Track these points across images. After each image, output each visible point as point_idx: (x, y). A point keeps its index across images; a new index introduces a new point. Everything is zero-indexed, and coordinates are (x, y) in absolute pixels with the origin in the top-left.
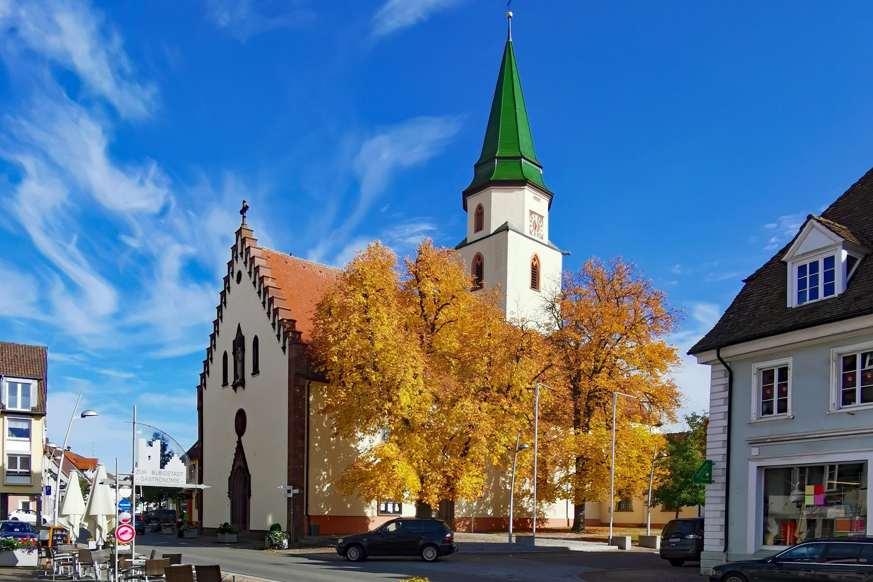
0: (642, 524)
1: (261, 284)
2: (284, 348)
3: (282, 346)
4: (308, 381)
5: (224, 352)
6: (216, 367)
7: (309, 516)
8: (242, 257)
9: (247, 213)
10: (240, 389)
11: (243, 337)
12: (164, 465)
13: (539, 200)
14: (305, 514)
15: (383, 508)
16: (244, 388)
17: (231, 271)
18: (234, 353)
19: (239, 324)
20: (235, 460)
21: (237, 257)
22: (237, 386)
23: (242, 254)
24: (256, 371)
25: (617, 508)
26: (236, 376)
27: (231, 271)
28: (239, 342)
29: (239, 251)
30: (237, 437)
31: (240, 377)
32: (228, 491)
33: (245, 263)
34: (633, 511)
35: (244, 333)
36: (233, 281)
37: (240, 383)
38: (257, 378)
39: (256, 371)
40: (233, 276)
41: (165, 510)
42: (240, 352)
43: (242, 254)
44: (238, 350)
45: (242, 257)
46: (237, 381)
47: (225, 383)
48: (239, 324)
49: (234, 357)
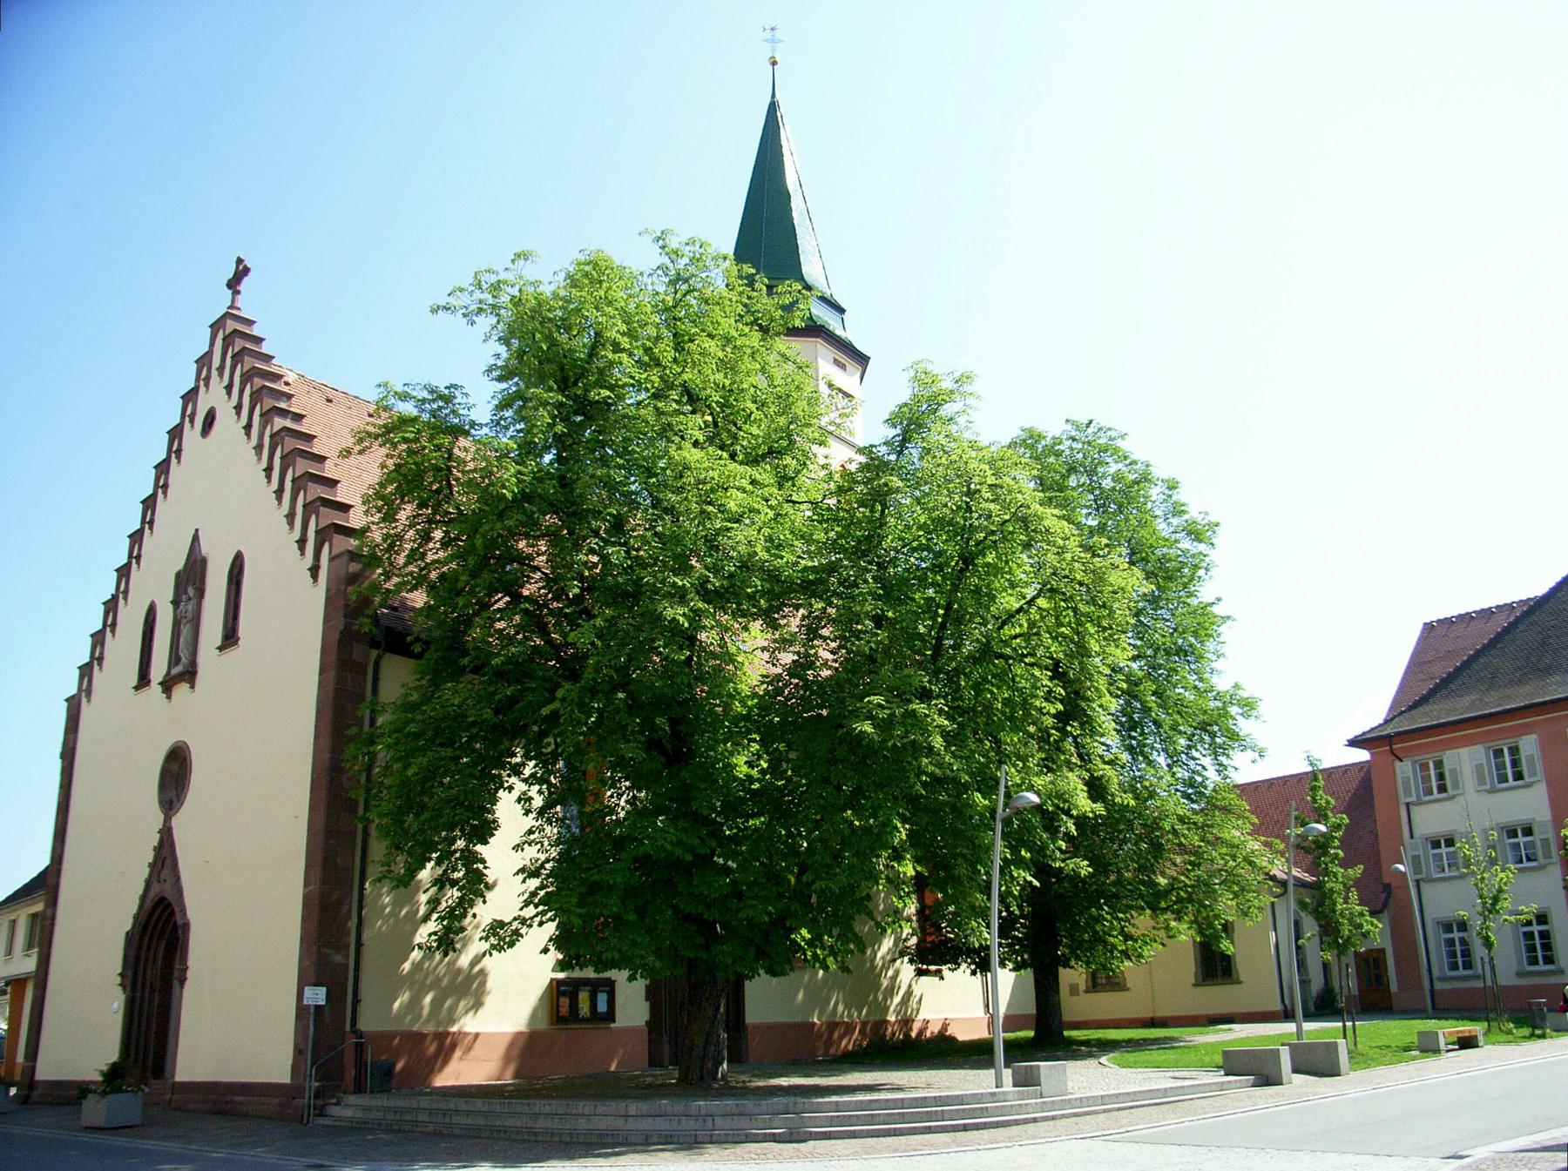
0: (1152, 1019)
1: (265, 428)
2: (314, 571)
3: (310, 566)
4: (374, 653)
5: (148, 603)
6: (124, 648)
7: (360, 1035)
8: (221, 375)
9: (245, 285)
10: (181, 690)
11: (204, 561)
12: (161, 841)
13: (843, 367)
14: (348, 1027)
15: (602, 999)
16: (192, 687)
17: (189, 412)
18: (176, 603)
19: (197, 530)
20: (148, 883)
21: (207, 380)
22: (176, 684)
23: (221, 369)
24: (230, 637)
25: (1090, 984)
26: (174, 658)
27: (189, 412)
28: (192, 576)
29: (216, 362)
30: (162, 817)
31: (184, 660)
32: (119, 971)
33: (229, 388)
34: (1128, 989)
35: (205, 548)
36: (191, 435)
37: (184, 673)
38: (232, 654)
39: (230, 637)
40: (192, 421)
41: (921, 931)
42: (190, 599)
43: (221, 369)
44: (186, 593)
45: (221, 375)
46: (176, 670)
47: (144, 680)
48: (197, 530)
49: (175, 611)
